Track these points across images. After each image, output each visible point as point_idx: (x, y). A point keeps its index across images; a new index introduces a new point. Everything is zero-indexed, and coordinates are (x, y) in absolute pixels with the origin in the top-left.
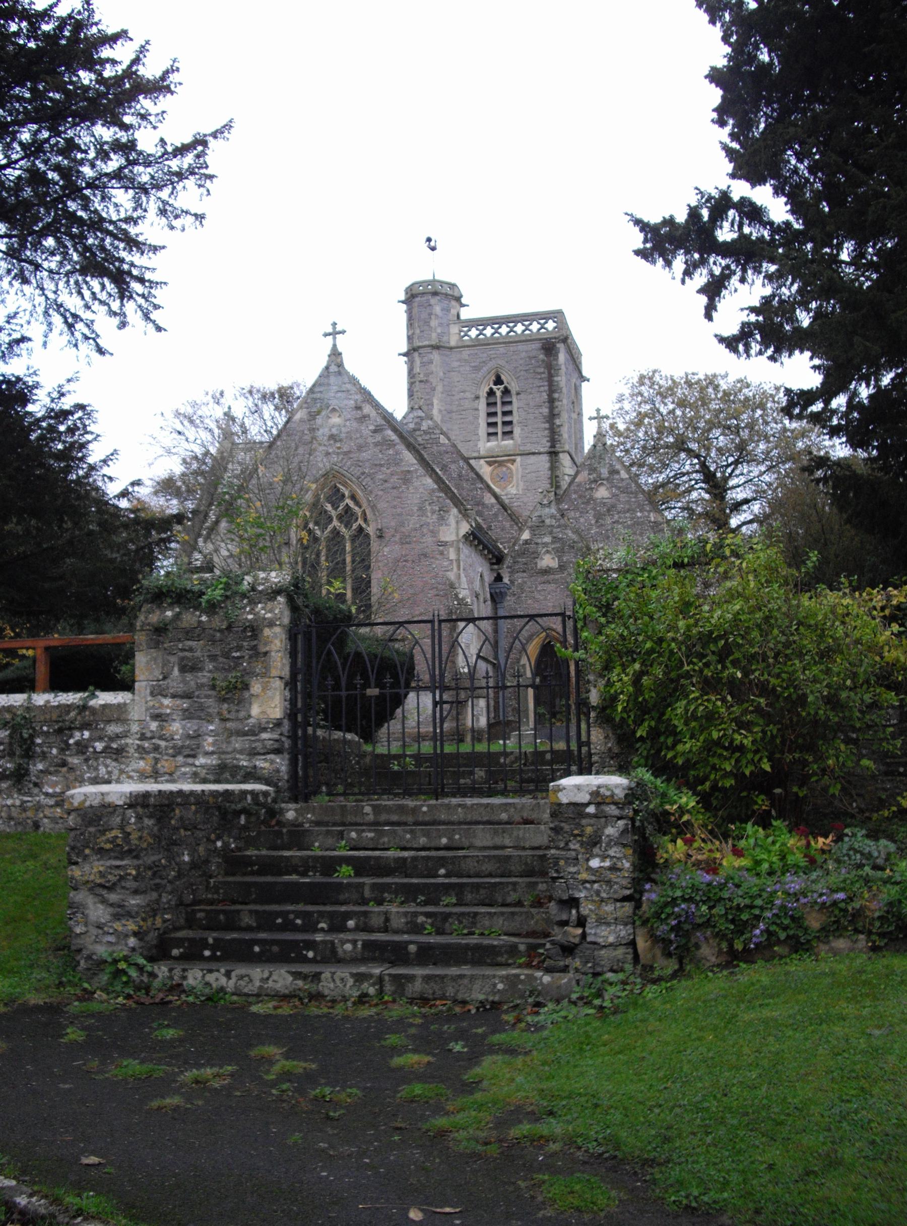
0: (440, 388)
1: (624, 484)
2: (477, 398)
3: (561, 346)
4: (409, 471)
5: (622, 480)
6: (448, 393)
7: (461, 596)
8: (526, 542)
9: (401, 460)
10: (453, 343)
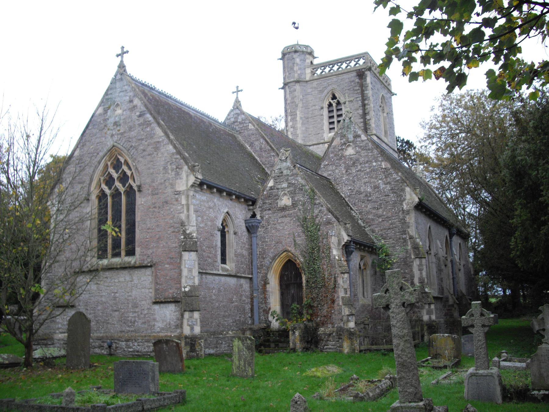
0: (300, 105)
1: (364, 144)
2: (322, 108)
4: (158, 142)
5: (363, 141)
6: (306, 107)
7: (188, 232)
8: (271, 188)
9: (154, 134)
10: (307, 79)
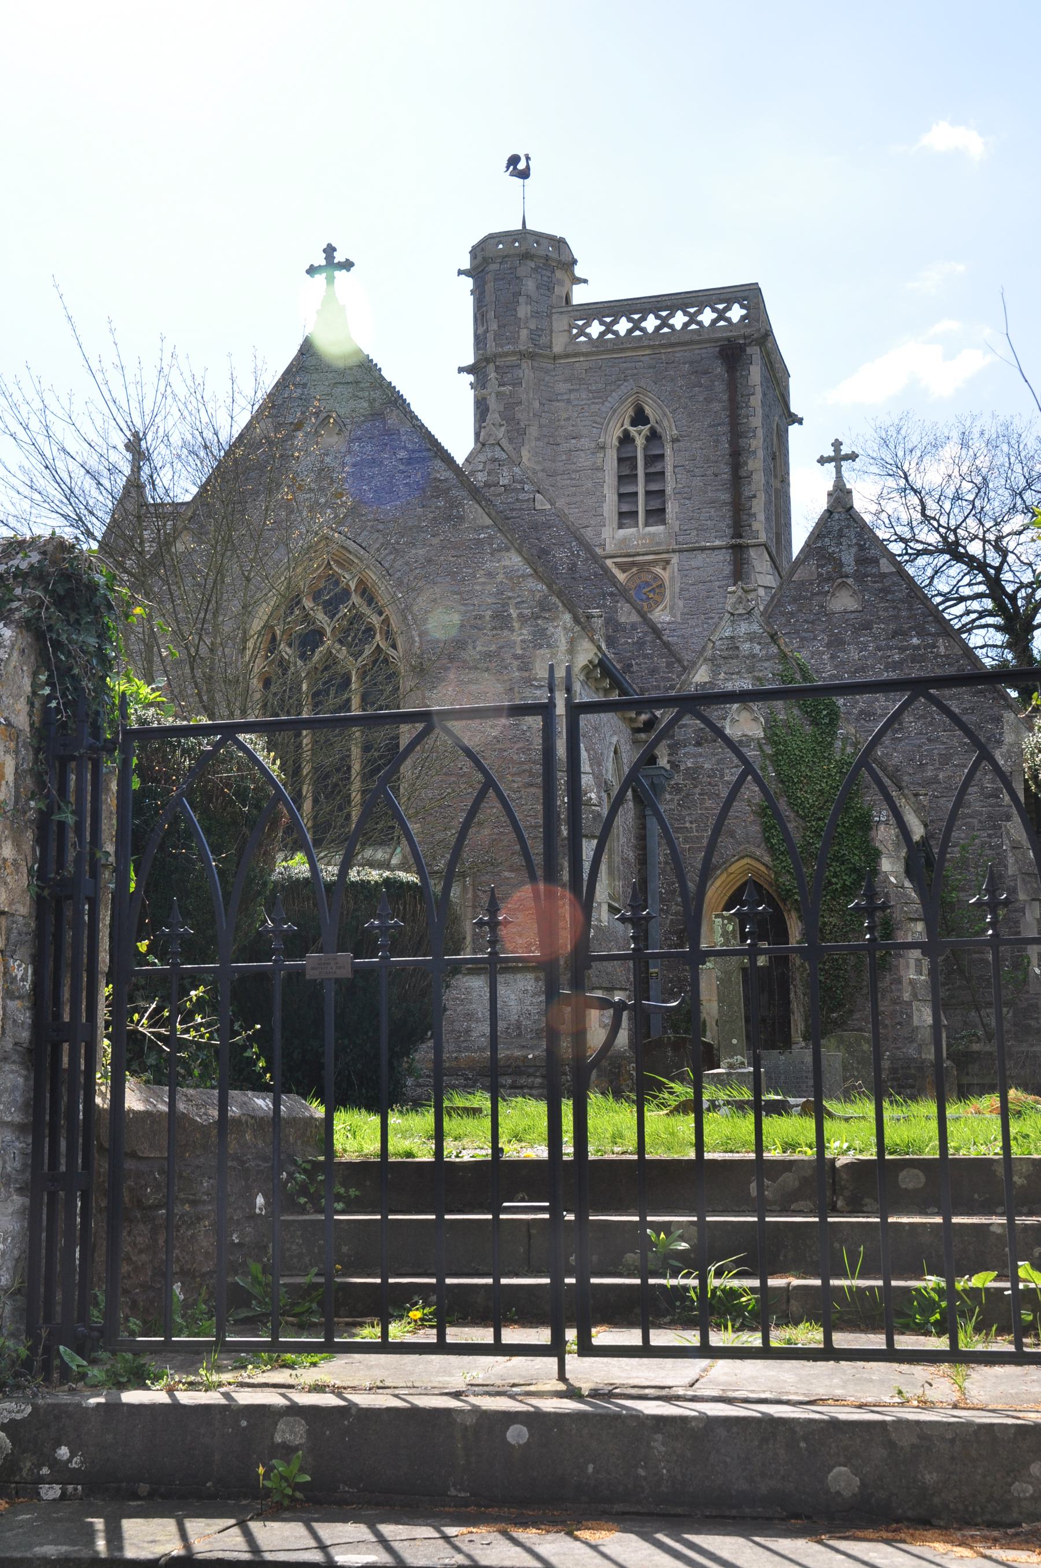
0: (533, 431)
3: (754, 351)
5: (884, 576)
